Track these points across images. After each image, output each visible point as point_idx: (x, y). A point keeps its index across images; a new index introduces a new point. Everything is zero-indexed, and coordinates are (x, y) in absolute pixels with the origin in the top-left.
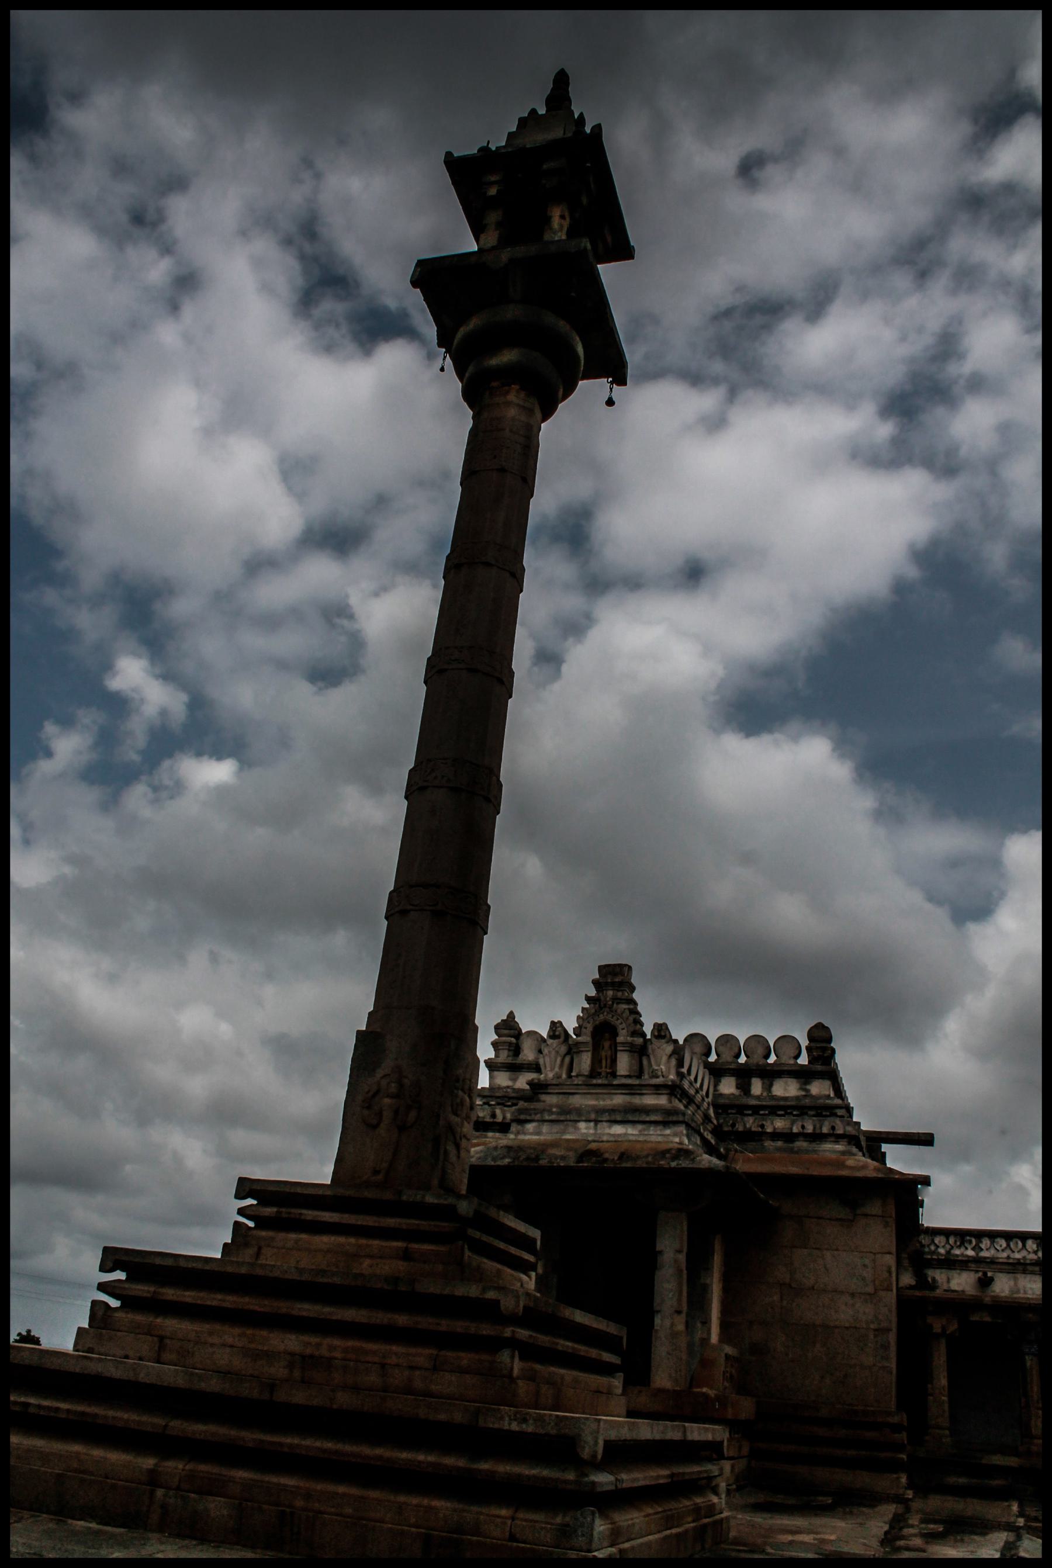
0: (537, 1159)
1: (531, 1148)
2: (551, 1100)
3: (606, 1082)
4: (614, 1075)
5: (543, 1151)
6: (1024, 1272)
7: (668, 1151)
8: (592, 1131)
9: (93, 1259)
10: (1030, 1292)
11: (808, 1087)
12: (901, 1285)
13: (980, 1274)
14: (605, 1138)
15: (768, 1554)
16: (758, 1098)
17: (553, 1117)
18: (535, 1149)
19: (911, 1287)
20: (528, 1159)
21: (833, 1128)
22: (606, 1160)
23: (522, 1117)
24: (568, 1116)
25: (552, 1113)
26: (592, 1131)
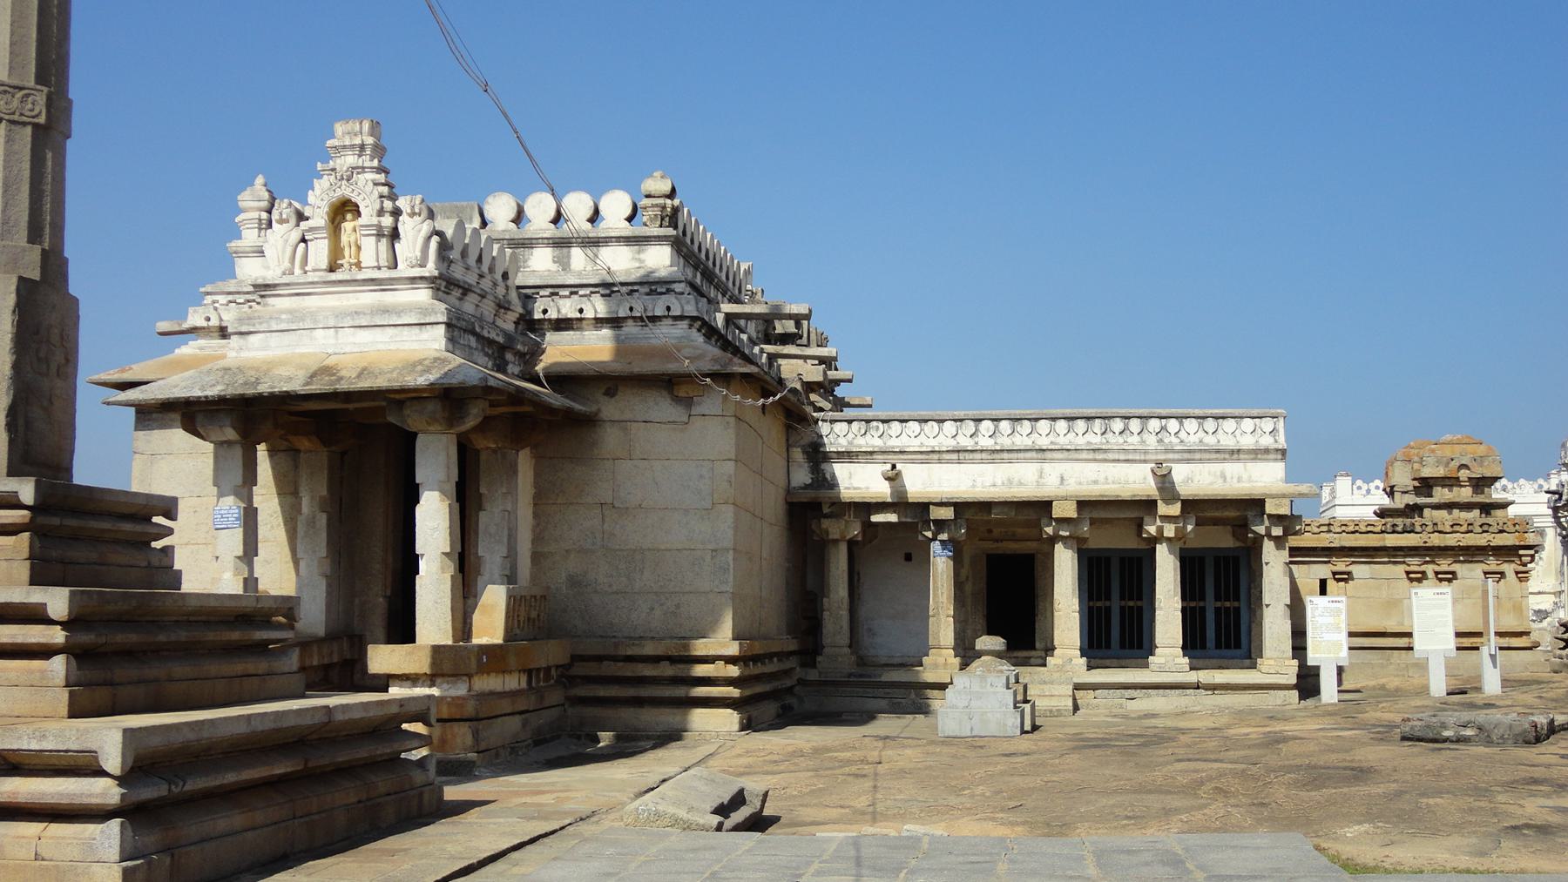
0: (257, 382)
1: (251, 368)
2: (278, 303)
3: (348, 277)
4: (358, 265)
5: (269, 370)
6: (940, 461)
7: (420, 362)
8: (332, 341)
9: (1343, 637)
10: (1072, 481)
11: (642, 256)
12: (794, 483)
13: (889, 467)
14: (347, 349)
15: (382, 683)
16: (579, 273)
17: (283, 326)
18: (257, 369)
19: (806, 487)
20: (246, 383)
21: (668, 308)
22: (341, 378)
23: (244, 329)
24: (298, 324)
25: (282, 321)
26: (332, 341)
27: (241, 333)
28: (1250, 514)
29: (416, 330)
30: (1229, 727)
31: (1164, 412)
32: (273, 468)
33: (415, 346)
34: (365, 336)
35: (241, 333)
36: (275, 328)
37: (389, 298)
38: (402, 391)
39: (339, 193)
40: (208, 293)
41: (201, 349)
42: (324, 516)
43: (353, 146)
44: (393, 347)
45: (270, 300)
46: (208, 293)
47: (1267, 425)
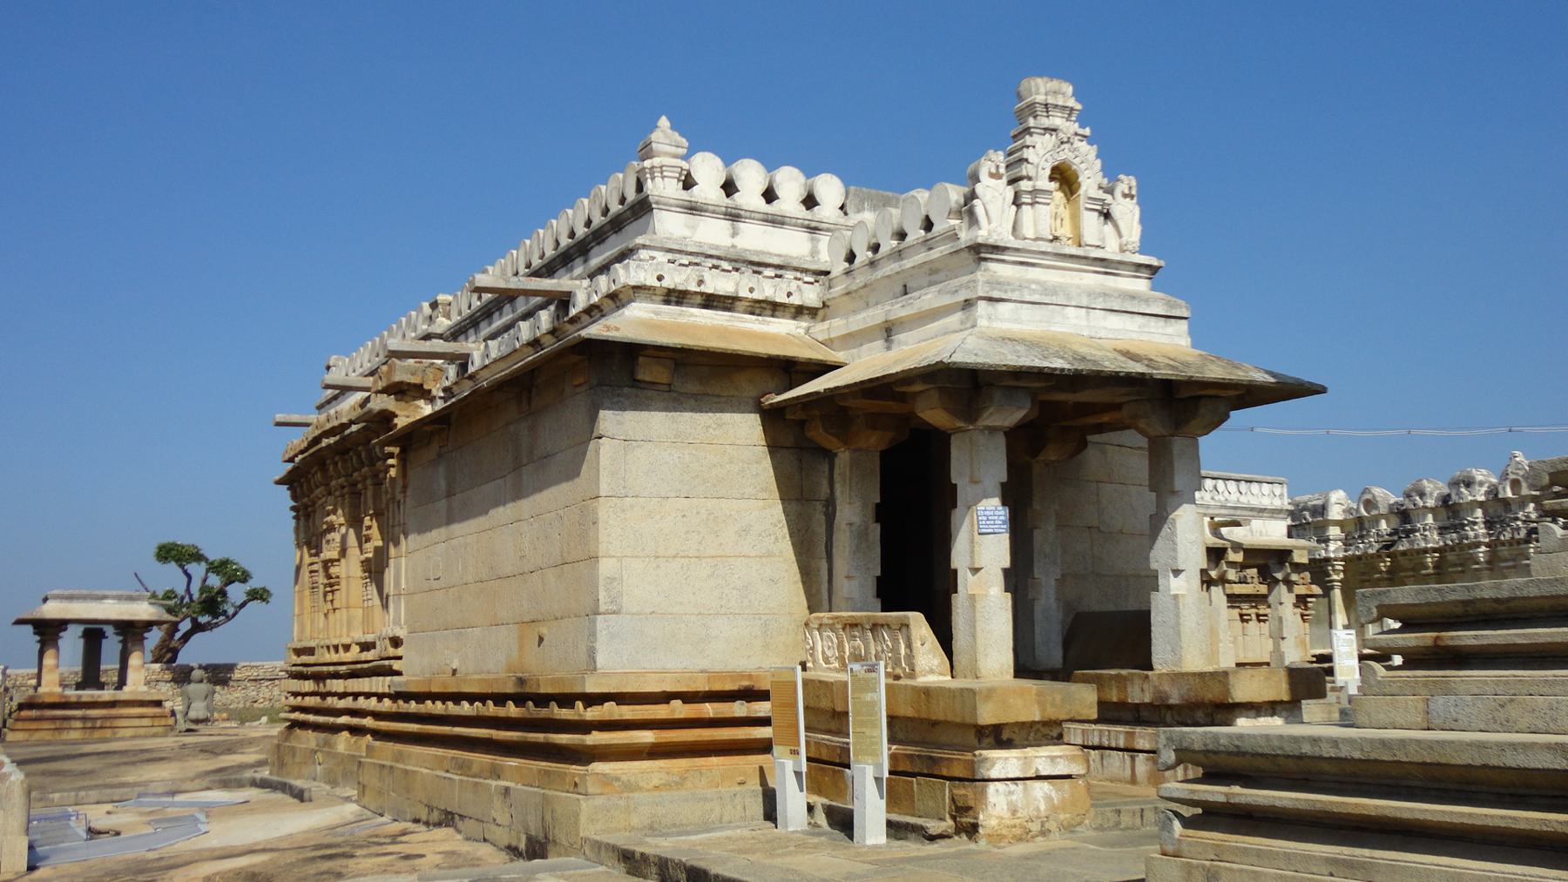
17: (1036, 298)
23: (995, 294)
26: (1084, 323)
27: (990, 299)
28: (1271, 562)
29: (1162, 321)
30: (878, 766)
31: (1216, 474)
32: (775, 468)
33: (1164, 340)
34: (1116, 321)
35: (990, 299)
36: (1028, 298)
37: (1111, 282)
38: (1191, 383)
39: (1062, 157)
40: (644, 247)
41: (657, 314)
42: (878, 526)
43: (1065, 107)
44: (1145, 337)
45: (992, 266)
46: (644, 247)
47: (1277, 489)
